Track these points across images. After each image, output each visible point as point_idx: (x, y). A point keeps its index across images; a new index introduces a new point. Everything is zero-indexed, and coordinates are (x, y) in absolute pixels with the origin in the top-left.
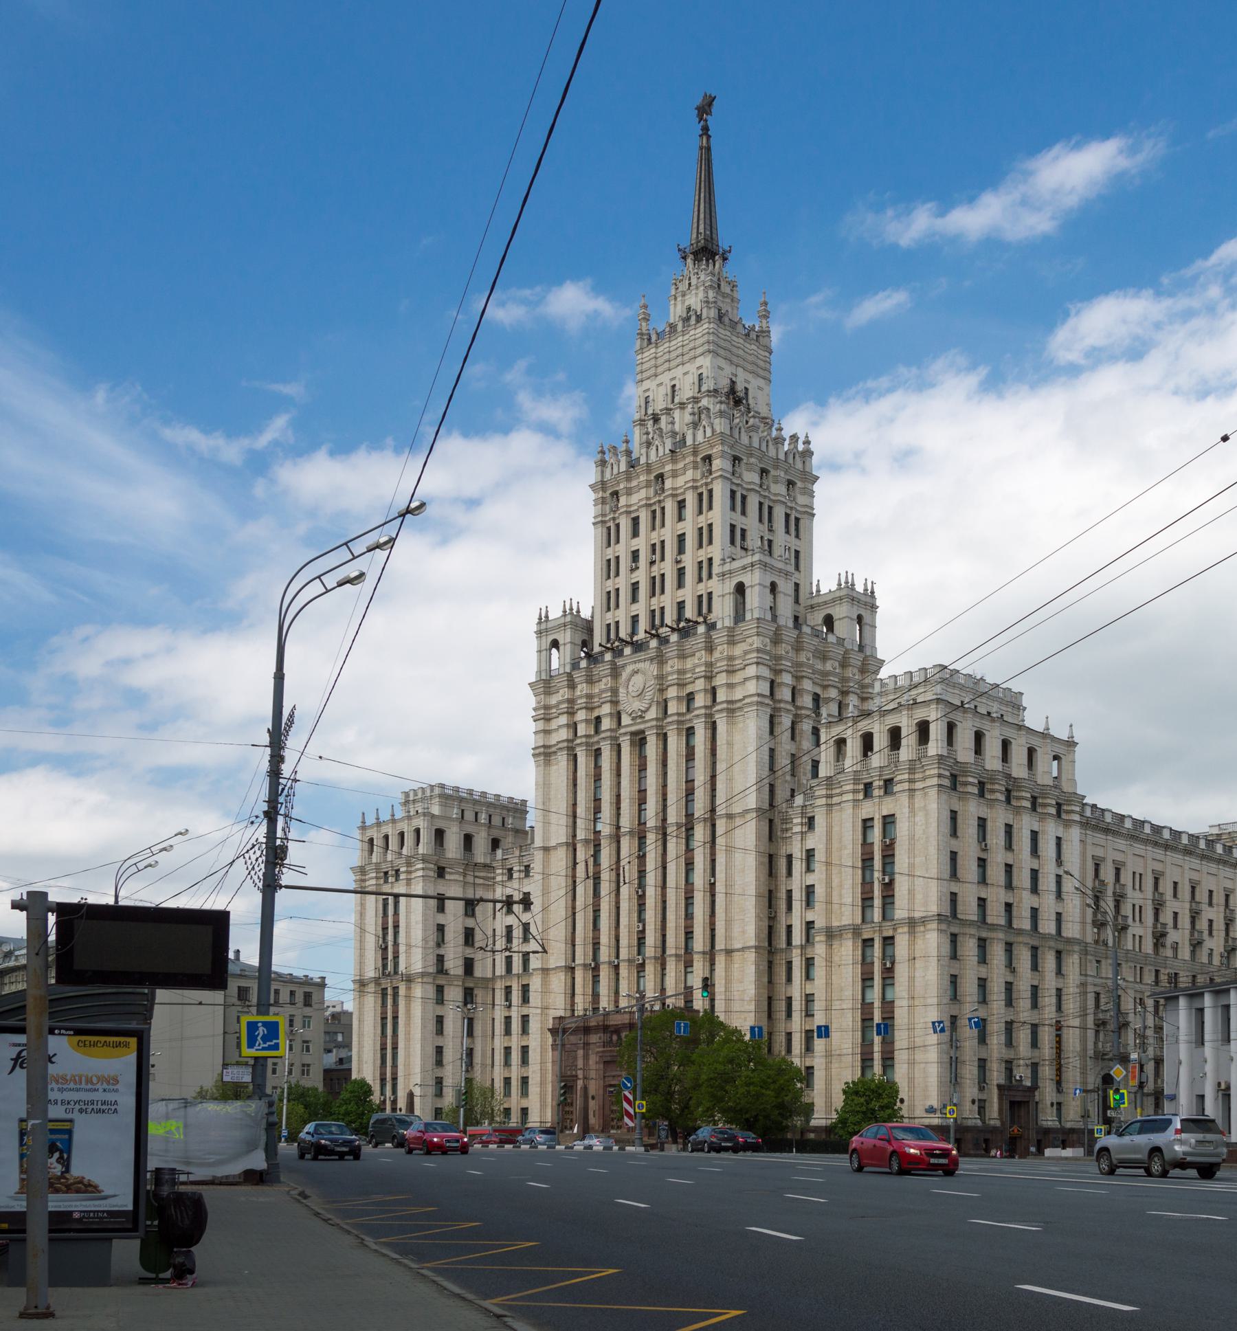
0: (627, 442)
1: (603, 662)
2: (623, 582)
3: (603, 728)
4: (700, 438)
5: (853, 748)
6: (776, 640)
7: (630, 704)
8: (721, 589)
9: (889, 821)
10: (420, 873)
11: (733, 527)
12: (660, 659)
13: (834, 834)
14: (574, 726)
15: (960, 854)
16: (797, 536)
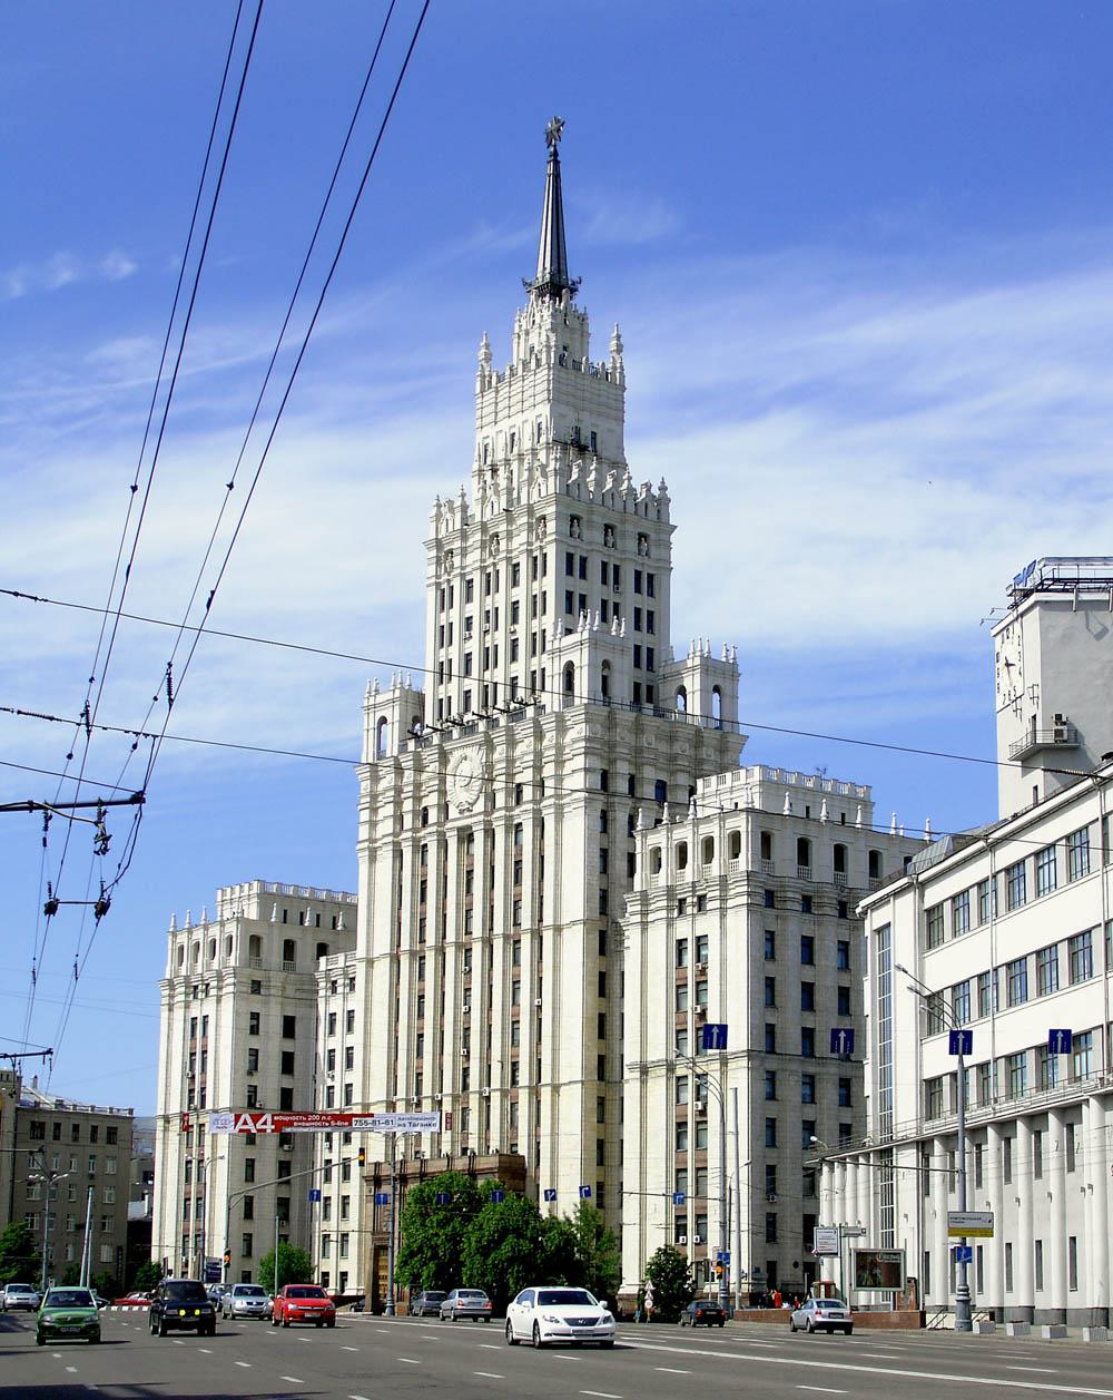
0: (463, 496)
1: (431, 745)
2: (454, 652)
3: (430, 822)
4: (535, 497)
5: (668, 858)
6: (611, 723)
7: (459, 795)
8: (554, 669)
9: (701, 941)
10: (231, 989)
11: (651, 594)
12: (489, 745)
13: (646, 956)
14: (399, 819)
15: (778, 979)
16: (651, 594)
